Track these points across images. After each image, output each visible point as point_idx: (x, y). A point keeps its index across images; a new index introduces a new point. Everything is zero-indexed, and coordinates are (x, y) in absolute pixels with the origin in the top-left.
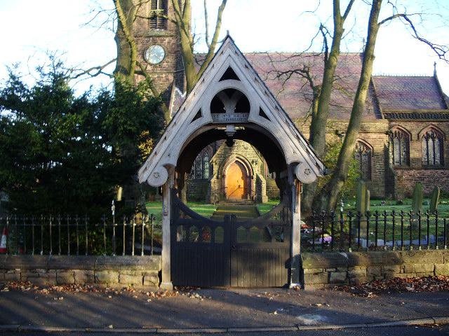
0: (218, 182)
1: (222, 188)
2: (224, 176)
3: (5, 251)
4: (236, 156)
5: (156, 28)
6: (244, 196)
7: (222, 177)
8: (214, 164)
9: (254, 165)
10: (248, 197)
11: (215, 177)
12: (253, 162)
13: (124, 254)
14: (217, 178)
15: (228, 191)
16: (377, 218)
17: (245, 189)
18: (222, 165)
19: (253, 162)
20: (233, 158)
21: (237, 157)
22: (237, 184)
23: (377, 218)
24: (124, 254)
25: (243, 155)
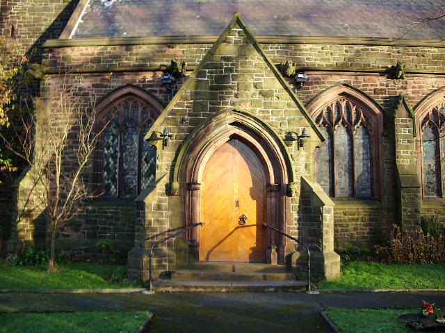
1: (188, 223)
6: (259, 254)
9: (292, 149)
10: (274, 255)
12: (289, 138)
17: (262, 228)
21: (235, 124)
25: (257, 115)
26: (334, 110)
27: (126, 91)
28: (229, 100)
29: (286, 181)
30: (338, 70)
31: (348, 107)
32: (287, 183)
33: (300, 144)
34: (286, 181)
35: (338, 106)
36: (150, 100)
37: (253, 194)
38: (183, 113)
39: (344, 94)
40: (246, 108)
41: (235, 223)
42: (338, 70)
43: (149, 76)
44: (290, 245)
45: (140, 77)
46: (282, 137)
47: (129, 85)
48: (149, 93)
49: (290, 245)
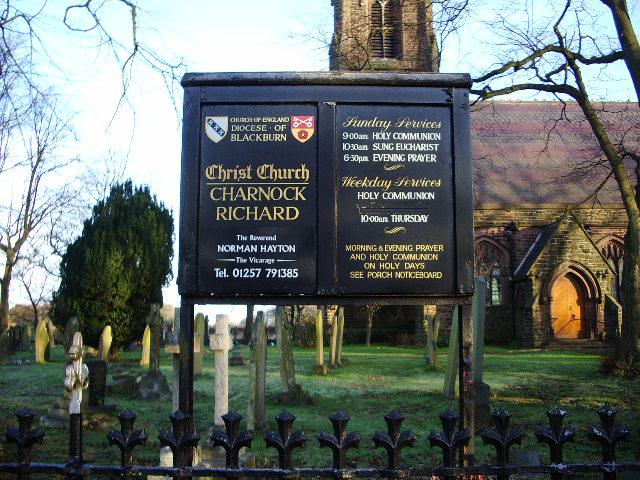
0: (541, 310)
1: (547, 318)
2: (550, 299)
3: (19, 478)
4: (569, 264)
5: (382, 57)
6: (583, 334)
7: (546, 301)
8: (533, 278)
9: (600, 281)
10: (592, 335)
11: (537, 300)
12: (598, 274)
13: (213, 370)
14: (541, 302)
15: (555, 325)
16: (502, 454)
17: (584, 319)
18: (547, 281)
19: (598, 274)
20: (564, 267)
21: (570, 267)
22: (570, 313)
23: (502, 454)
24: (213, 370)
25: (582, 262)
26: (607, 250)
27: (481, 240)
28: (567, 255)
29: (597, 296)
30: (605, 225)
31: (614, 248)
32: (78, 411)
33: (604, 277)
34: (597, 296)
35: (609, 247)
36: (497, 245)
37: (579, 303)
38: (545, 262)
39: (613, 240)
40: (577, 259)
41: (570, 318)
42: (605, 225)
43: (496, 230)
44: (601, 327)
45: (490, 231)
46: (595, 273)
47: (485, 236)
48: (498, 241)
49: (601, 327)
